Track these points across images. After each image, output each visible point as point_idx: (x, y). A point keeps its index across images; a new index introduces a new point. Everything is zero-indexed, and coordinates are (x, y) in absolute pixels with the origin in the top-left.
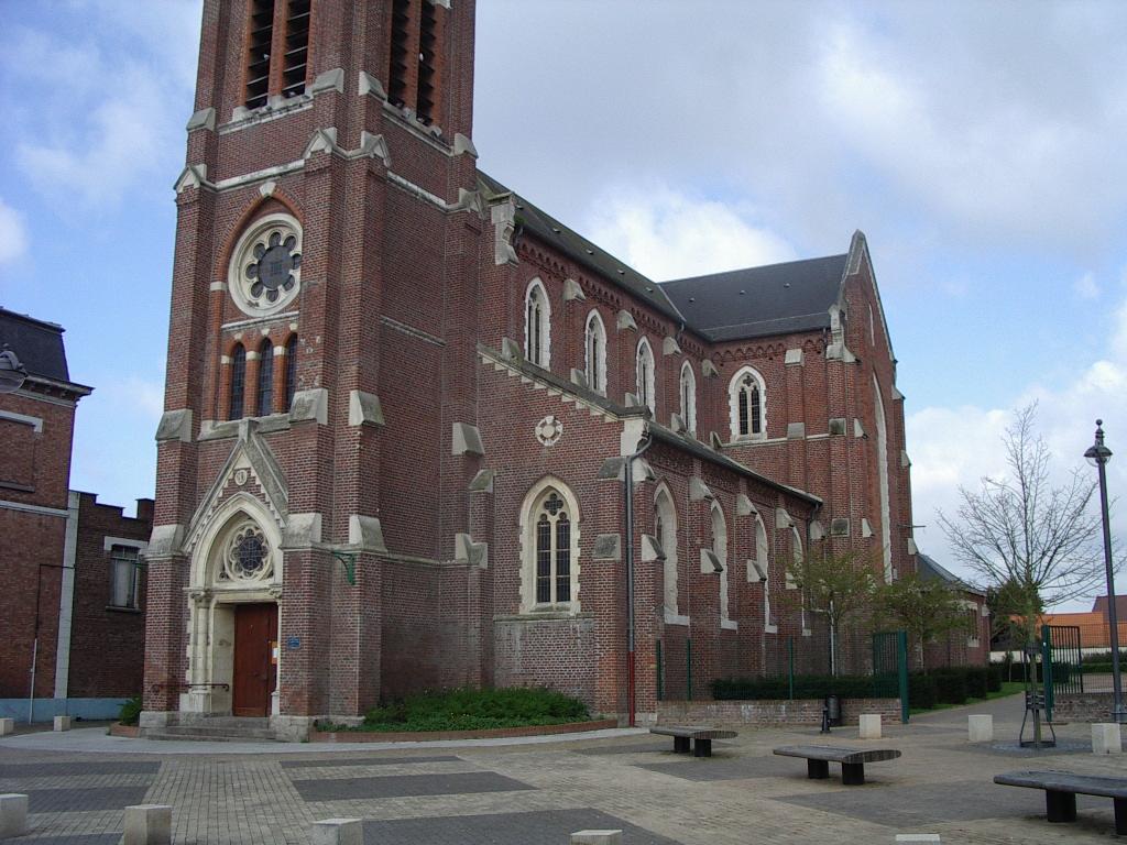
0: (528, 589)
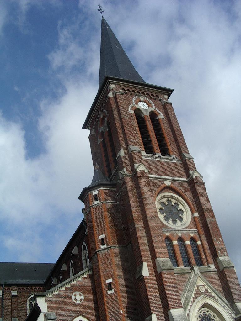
0: (163, 229)
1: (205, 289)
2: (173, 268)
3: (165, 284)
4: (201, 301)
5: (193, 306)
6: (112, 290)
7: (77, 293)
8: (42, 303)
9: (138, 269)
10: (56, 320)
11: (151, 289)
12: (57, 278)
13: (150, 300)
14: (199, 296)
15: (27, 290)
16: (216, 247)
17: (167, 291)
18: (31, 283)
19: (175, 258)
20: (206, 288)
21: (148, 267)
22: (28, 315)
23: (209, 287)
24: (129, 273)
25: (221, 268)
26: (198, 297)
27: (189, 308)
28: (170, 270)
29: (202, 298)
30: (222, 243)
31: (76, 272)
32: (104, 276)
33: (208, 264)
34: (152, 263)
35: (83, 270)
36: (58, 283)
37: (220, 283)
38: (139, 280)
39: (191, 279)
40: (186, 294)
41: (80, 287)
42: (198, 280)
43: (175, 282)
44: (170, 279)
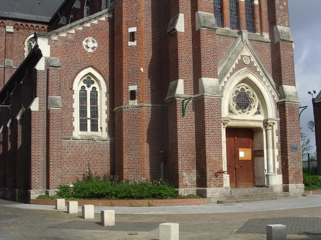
1: (250, 62)
2: (216, 27)
3: (202, 46)
4: (242, 75)
5: (231, 78)
6: (134, 41)
7: (90, 39)
8: (44, 45)
9: (171, 21)
10: (60, 68)
11: (183, 48)
12: (66, 17)
13: (180, 61)
14: (241, 68)
15: (27, 27)
16: (277, 12)
17: (203, 54)
18: (31, 19)
19: (221, 16)
20: (252, 60)
21: (184, 20)
22: (25, 57)
23: (256, 59)
24: (160, 23)
25: (276, 40)
26: (240, 68)
27: (226, 79)
28: (212, 29)
29: (244, 71)
30: (286, 10)
31: (91, 12)
32: (127, 22)
33: (262, 31)
34: (190, 16)
35: (100, 10)
36: (67, 23)
37: (271, 58)
38: (171, 34)
39: (236, 46)
40: (226, 62)
41: (94, 32)
42: (245, 49)
43: (215, 46)
44: (210, 40)
